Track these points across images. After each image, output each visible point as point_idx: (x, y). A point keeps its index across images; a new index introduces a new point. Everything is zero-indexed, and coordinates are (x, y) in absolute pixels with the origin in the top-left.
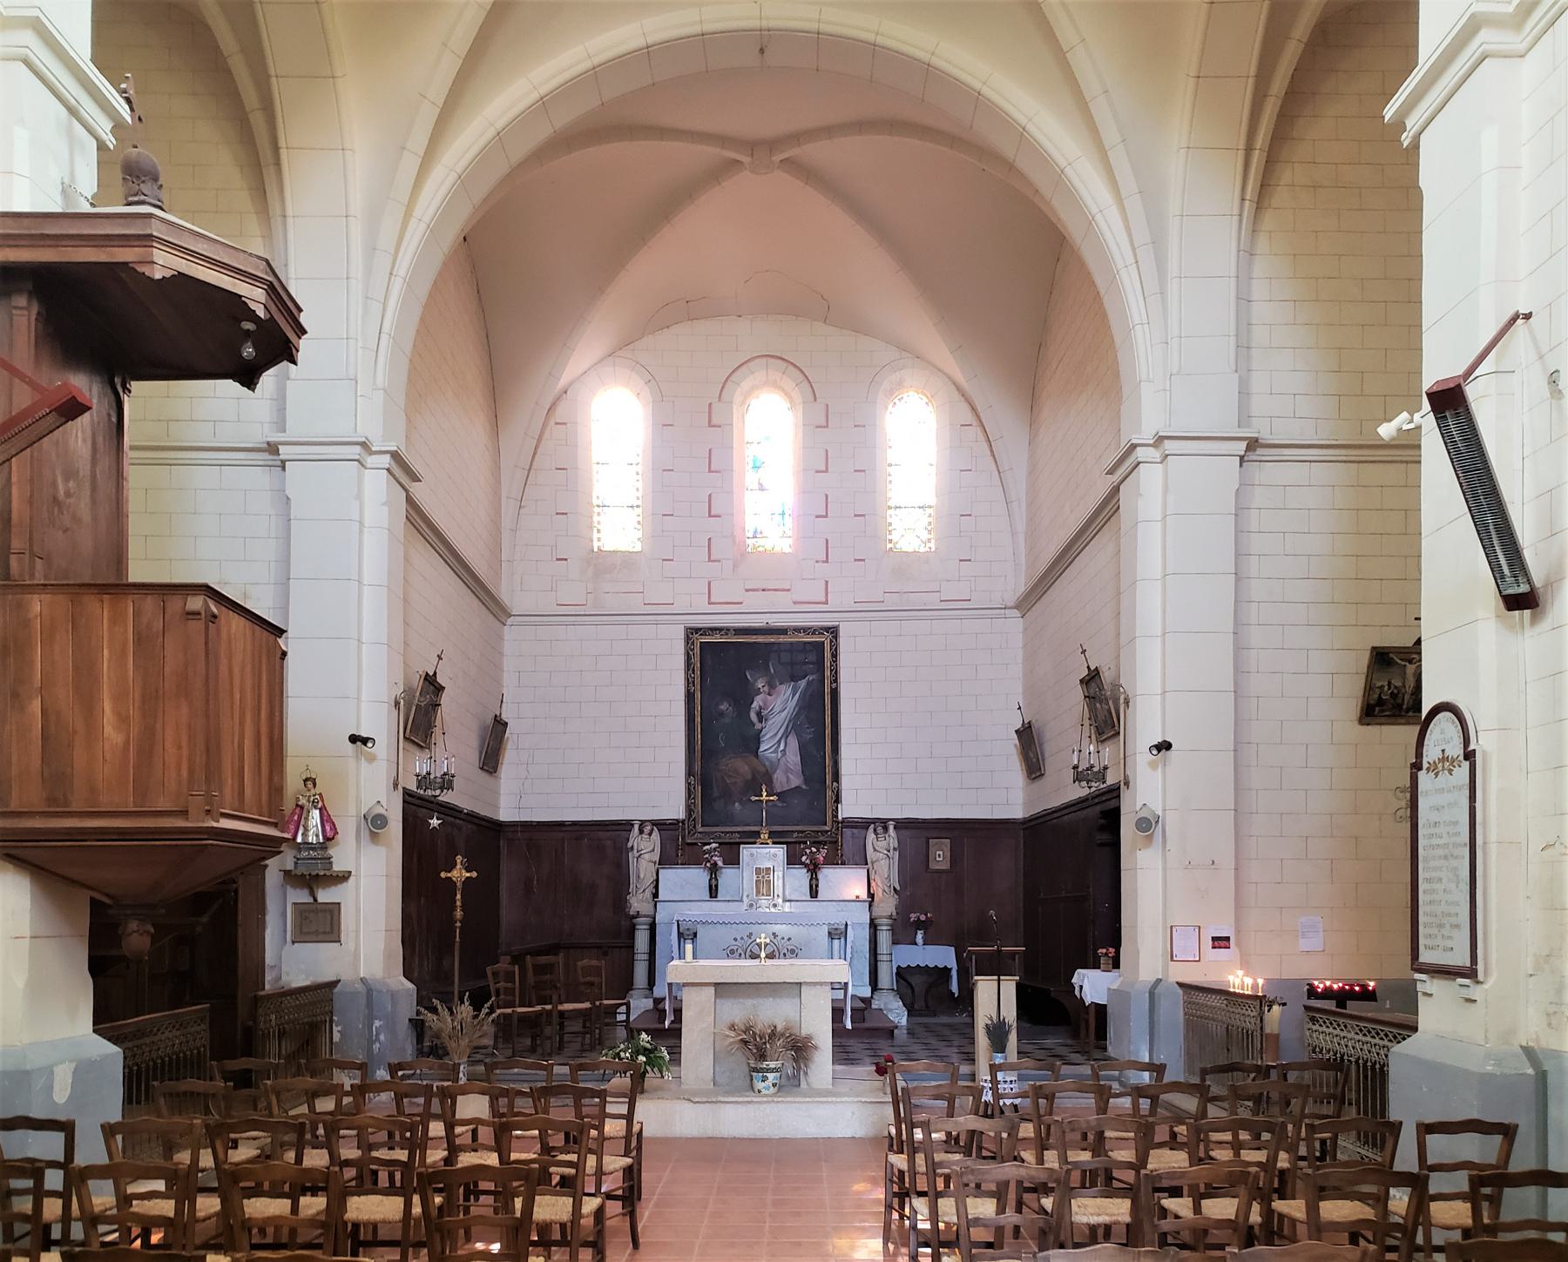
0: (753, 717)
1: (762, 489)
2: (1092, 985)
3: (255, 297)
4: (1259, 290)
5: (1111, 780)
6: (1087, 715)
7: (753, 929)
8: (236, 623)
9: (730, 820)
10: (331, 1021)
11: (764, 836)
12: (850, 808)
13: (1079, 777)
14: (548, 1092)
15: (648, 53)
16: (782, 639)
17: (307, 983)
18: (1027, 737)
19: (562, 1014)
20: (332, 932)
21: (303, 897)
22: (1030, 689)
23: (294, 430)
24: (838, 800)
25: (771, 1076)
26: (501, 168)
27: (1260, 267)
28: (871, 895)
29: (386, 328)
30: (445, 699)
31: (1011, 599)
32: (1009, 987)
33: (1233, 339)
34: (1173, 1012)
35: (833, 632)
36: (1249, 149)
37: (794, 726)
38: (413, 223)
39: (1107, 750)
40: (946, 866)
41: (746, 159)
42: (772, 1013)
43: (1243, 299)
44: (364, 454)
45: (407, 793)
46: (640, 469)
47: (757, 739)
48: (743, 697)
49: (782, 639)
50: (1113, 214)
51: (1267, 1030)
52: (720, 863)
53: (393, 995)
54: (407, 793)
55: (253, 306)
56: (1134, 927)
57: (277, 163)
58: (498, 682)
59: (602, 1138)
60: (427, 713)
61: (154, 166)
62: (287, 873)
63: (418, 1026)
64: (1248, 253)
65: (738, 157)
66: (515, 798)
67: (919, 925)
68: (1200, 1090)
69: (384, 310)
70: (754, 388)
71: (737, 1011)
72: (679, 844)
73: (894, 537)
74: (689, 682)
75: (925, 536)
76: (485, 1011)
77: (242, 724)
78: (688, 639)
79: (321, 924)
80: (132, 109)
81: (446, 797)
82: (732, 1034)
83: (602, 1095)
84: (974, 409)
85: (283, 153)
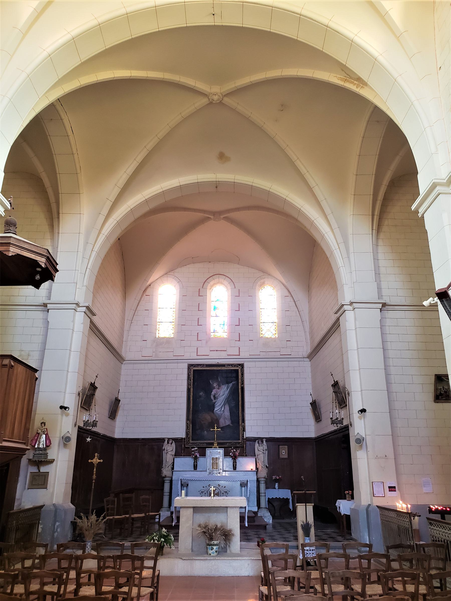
0: (212, 397)
1: (216, 316)
2: (344, 506)
3: (42, 261)
4: (381, 256)
5: (345, 423)
6: (334, 398)
7: (211, 483)
8: (20, 369)
9: (202, 438)
10: (39, 523)
11: (216, 445)
12: (250, 433)
13: (333, 422)
14: (122, 557)
15: (181, 187)
16: (223, 368)
17: (31, 506)
18: (314, 405)
19: (133, 519)
20: (44, 484)
21: (34, 469)
22: (314, 388)
23: (53, 300)
24: (244, 430)
25: (215, 547)
26: (132, 219)
27: (381, 249)
28: (257, 469)
29: (89, 267)
30: (97, 393)
31: (306, 354)
32: (310, 508)
33: (373, 271)
34: (376, 519)
35: (242, 366)
36: (373, 215)
37: (228, 401)
38: (101, 235)
39: (343, 412)
40: (286, 456)
41: (212, 217)
42: (216, 520)
43: (376, 259)
44: (77, 307)
45: (79, 428)
46: (174, 310)
47: (213, 406)
48: (208, 390)
49: (223, 368)
50: (330, 234)
51: (414, 528)
52: (198, 456)
53: (66, 511)
54: (79, 428)
55: (41, 263)
56: (358, 482)
57: (58, 218)
58: (118, 385)
59: (141, 579)
60: (90, 398)
61: (16, 222)
62: (30, 460)
63: (74, 525)
64: (376, 245)
65: (210, 216)
66: (121, 430)
67: (276, 481)
68: (386, 556)
69: (89, 261)
70: (215, 284)
71: (201, 519)
72: (183, 448)
73: (263, 332)
74: (189, 384)
75: (274, 332)
76: (101, 518)
77: (17, 405)
78: (189, 368)
79: (40, 481)
80: (11, 206)
81: (94, 429)
82: (199, 529)
83: (142, 559)
84: (289, 291)
85: (61, 215)
